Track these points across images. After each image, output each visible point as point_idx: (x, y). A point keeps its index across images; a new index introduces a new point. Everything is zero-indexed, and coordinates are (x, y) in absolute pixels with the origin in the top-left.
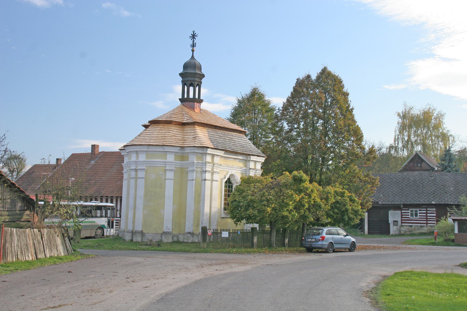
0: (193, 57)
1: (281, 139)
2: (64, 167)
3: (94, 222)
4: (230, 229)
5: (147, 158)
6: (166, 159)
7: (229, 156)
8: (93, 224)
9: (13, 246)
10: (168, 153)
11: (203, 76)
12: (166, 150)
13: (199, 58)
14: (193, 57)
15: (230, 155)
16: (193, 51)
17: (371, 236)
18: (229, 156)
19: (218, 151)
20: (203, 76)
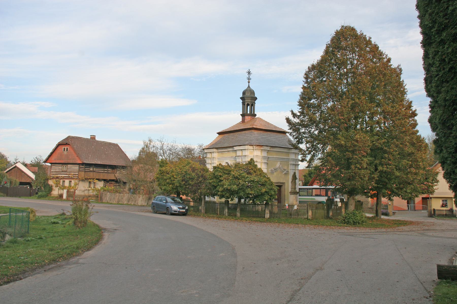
0: (249, 86)
1: (335, 131)
2: (241, 159)
3: (314, 199)
4: (91, 136)
5: (267, 155)
6: (289, 157)
7: (224, 151)
8: (313, 200)
9: (383, 233)
10: (237, 151)
11: (256, 98)
12: (235, 149)
13: (252, 87)
14: (249, 86)
15: (222, 149)
16: (249, 82)
17: (282, 202)
18: (224, 151)
19: (276, 148)
20: (256, 98)
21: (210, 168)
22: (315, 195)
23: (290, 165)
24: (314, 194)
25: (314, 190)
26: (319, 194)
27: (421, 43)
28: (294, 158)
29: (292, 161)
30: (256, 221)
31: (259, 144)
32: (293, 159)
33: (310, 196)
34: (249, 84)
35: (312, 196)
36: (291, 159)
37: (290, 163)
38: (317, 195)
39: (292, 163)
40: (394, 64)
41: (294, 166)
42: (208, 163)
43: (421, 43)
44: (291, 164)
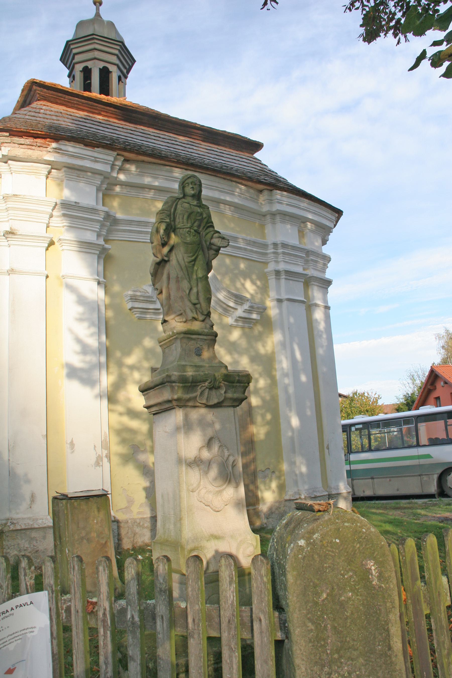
3: (428, 456)
8: (422, 461)
21: (182, 604)
22: (430, 440)
23: (272, 282)
24: (424, 440)
25: (422, 427)
26: (442, 435)
27: (91, 69)
28: (294, 241)
29: (281, 258)
30: (130, 106)
31: (38, 214)
32: (284, 245)
33: (410, 447)
34: (98, 9)
35: (418, 445)
36: (275, 245)
37: (271, 267)
38: (434, 442)
39: (282, 267)
40: (90, 67)
41: (299, 286)
42: (146, 527)
43: (91, 69)
44: (278, 273)
